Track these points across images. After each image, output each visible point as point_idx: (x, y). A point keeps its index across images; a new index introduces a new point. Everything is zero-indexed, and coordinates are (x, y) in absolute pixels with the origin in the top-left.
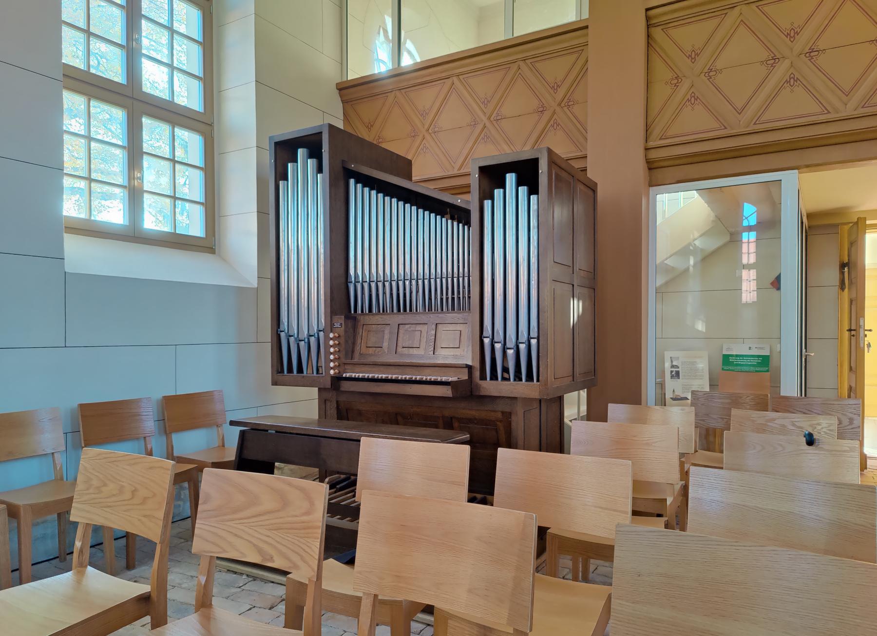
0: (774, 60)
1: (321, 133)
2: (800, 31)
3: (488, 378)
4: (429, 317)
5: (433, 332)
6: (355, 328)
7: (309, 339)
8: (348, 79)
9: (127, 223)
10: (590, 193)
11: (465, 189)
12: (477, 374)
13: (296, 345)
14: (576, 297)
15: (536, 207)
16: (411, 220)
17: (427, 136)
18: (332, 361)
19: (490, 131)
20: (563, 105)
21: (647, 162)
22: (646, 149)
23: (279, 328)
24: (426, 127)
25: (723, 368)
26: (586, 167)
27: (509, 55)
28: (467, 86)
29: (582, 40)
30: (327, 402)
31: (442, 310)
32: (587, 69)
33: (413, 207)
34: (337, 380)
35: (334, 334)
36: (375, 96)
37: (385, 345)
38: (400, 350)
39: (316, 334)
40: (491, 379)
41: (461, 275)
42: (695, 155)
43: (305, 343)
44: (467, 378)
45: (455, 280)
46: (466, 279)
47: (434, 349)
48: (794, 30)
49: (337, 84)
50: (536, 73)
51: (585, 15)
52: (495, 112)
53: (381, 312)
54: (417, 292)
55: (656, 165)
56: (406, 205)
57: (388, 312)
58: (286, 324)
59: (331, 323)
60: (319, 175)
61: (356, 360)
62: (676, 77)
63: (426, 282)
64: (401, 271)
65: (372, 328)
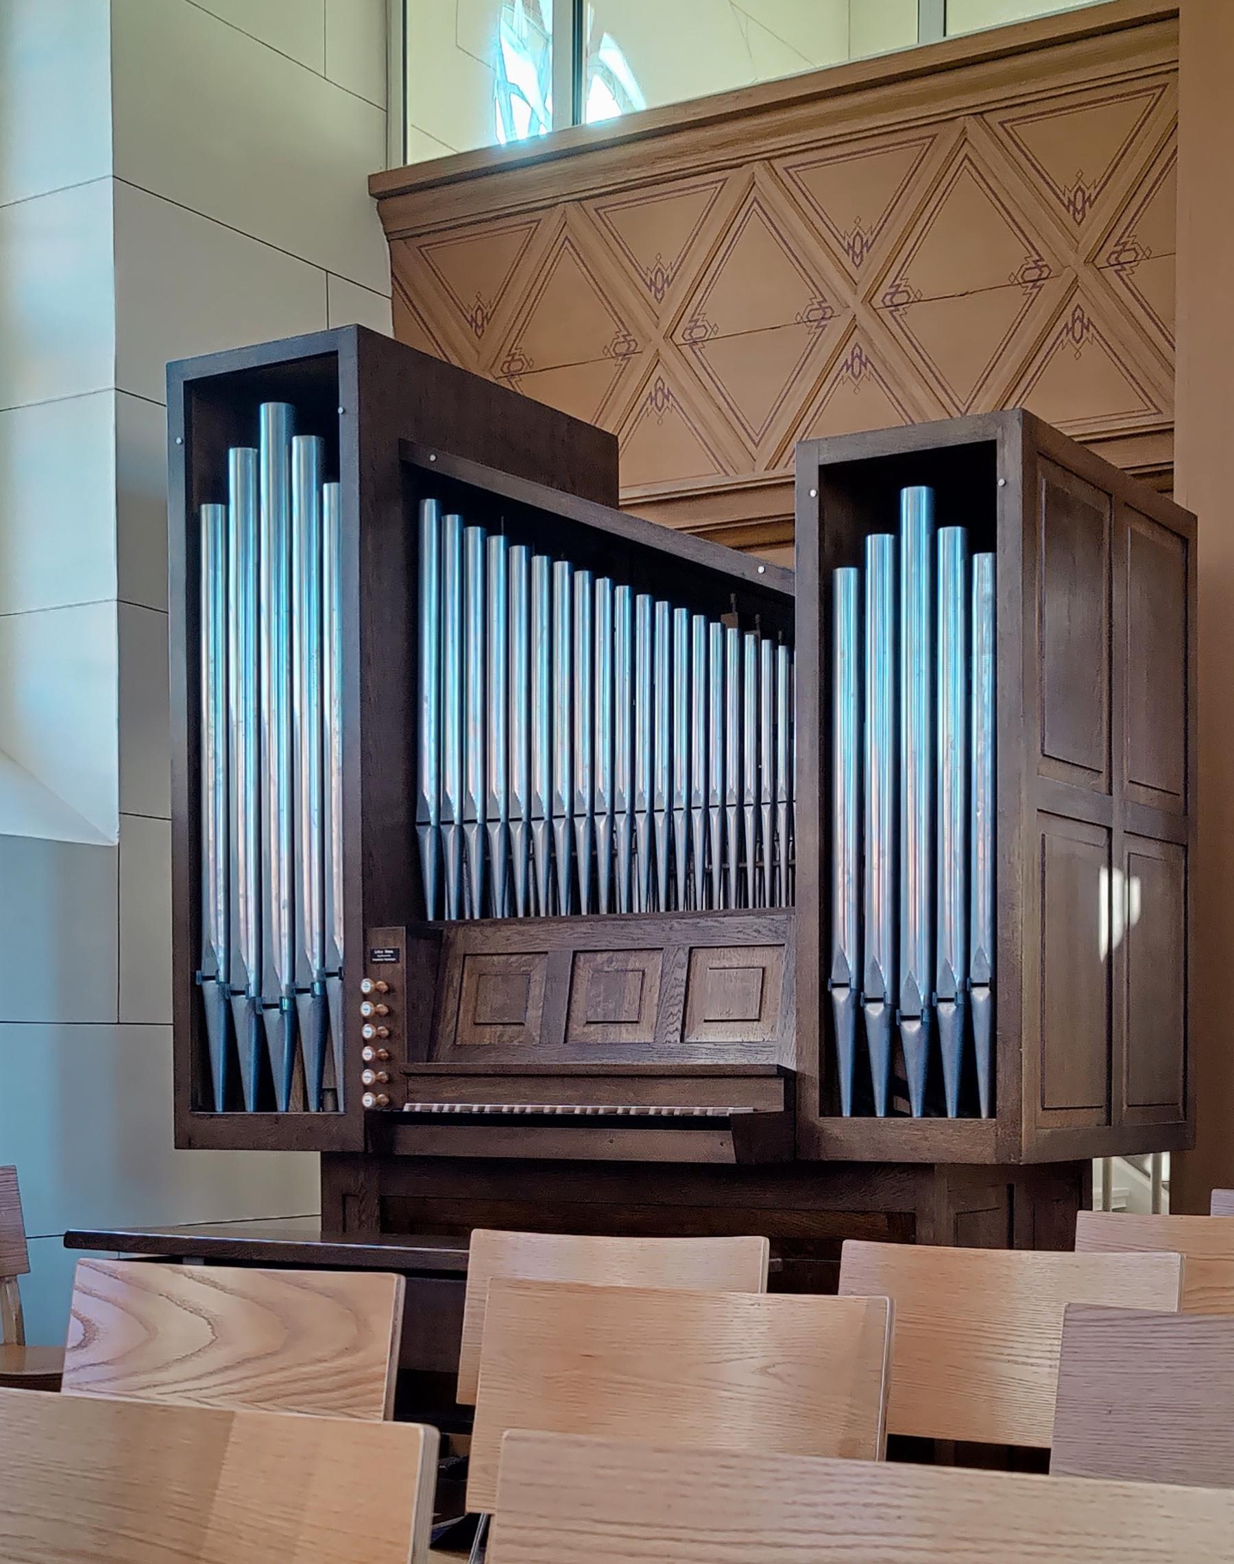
3: (846, 1111)
4: (667, 927)
5: (683, 974)
6: (438, 967)
7: (293, 1002)
8: (410, 162)
10: (1171, 545)
12: (812, 1096)
13: (253, 1020)
14: (1120, 868)
17: (668, 354)
18: (366, 1065)
19: (871, 343)
20: (1101, 261)
23: (200, 968)
24: (666, 324)
26: (1172, 463)
27: (934, 96)
30: (349, 1199)
32: (1175, 151)
35: (375, 982)
36: (497, 218)
37: (533, 1015)
38: (577, 1030)
39: (317, 986)
40: (855, 1112)
43: (282, 1012)
44: (781, 1108)
46: (782, 809)
47: (684, 1025)
49: (370, 177)
52: (888, 281)
53: (521, 914)
54: (633, 852)
56: (599, 582)
57: (543, 914)
58: (221, 954)
60: (325, 486)
61: (443, 1062)
63: (660, 819)
64: (584, 787)
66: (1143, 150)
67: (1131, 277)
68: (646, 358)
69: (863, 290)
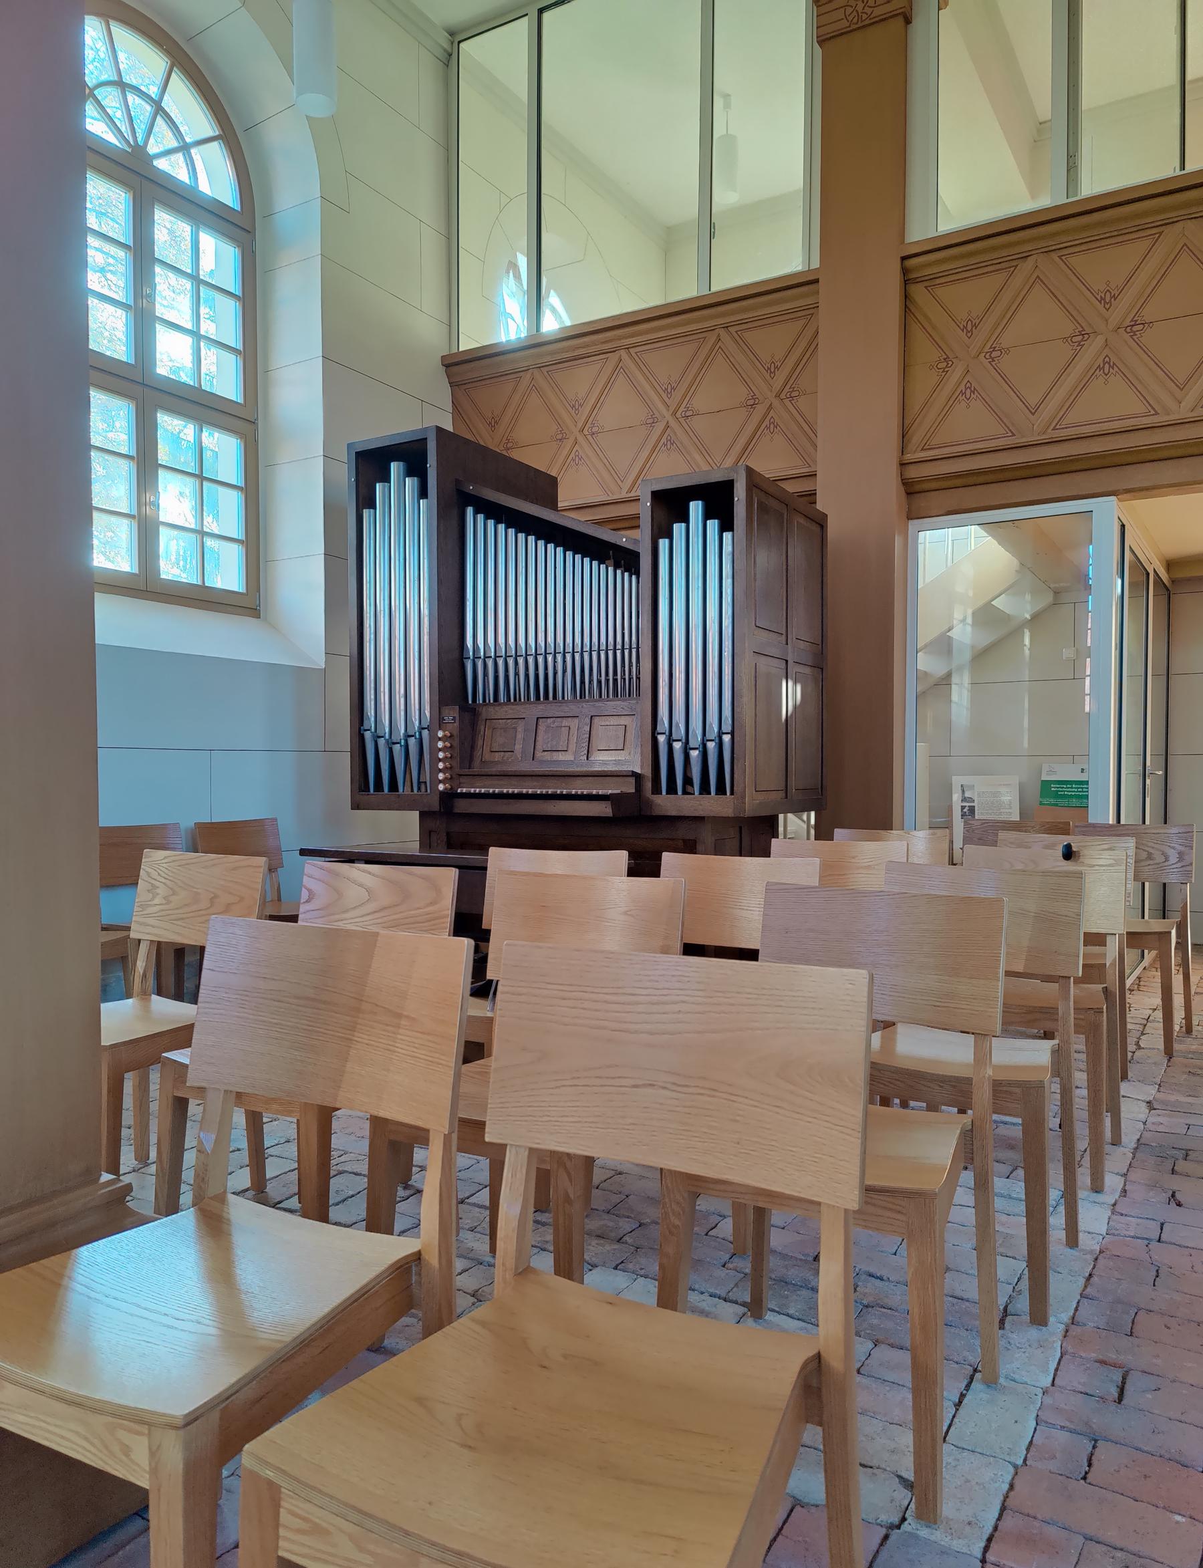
0: (1083, 336)
1: (426, 438)
2: (1119, 295)
3: (664, 792)
6: (474, 725)
8: (460, 350)
9: (136, 570)
11: (632, 522)
12: (648, 785)
14: (792, 679)
15: (730, 548)
16: (555, 568)
17: (581, 439)
19: (675, 433)
20: (783, 396)
21: (903, 483)
22: (902, 465)
23: (363, 726)
24: (580, 425)
25: (1041, 802)
28: (642, 366)
29: (809, 301)
31: (600, 696)
32: (817, 345)
33: (558, 549)
34: (448, 797)
37: (518, 747)
38: (539, 754)
39: (417, 733)
41: (627, 646)
42: (1002, 469)
43: (401, 746)
44: (633, 791)
45: (619, 653)
46: (634, 651)
48: (1110, 293)
49: (442, 357)
50: (744, 346)
51: (816, 264)
52: (683, 405)
53: (512, 700)
54: (564, 671)
55: (917, 488)
56: (549, 545)
58: (373, 719)
59: (440, 718)
62: (945, 359)
63: (577, 656)
64: (542, 641)
65: (500, 724)
66: (803, 344)
67: (1140, 339)
68: (571, 441)
69: (672, 409)
